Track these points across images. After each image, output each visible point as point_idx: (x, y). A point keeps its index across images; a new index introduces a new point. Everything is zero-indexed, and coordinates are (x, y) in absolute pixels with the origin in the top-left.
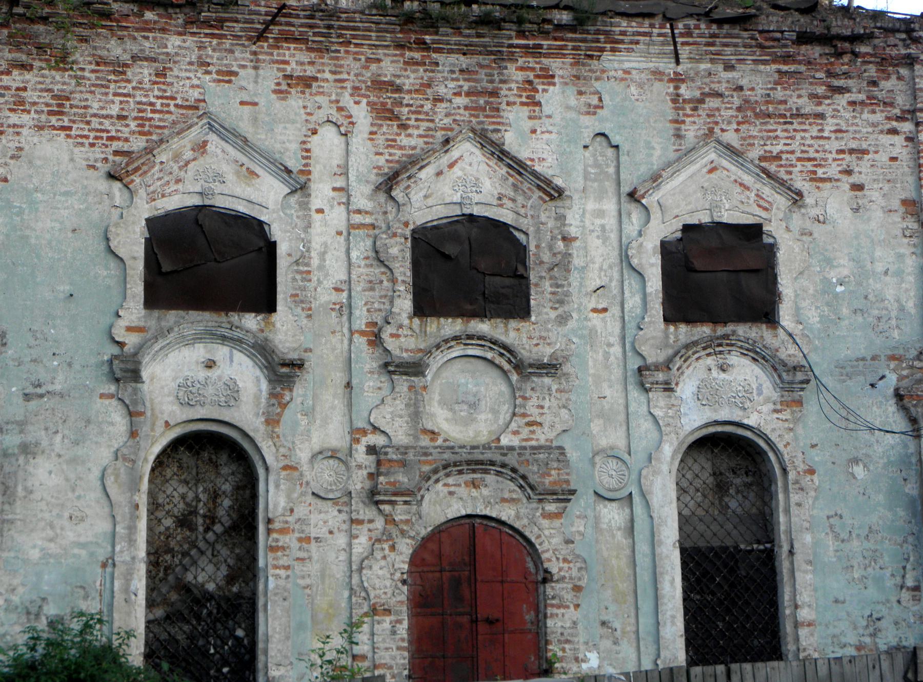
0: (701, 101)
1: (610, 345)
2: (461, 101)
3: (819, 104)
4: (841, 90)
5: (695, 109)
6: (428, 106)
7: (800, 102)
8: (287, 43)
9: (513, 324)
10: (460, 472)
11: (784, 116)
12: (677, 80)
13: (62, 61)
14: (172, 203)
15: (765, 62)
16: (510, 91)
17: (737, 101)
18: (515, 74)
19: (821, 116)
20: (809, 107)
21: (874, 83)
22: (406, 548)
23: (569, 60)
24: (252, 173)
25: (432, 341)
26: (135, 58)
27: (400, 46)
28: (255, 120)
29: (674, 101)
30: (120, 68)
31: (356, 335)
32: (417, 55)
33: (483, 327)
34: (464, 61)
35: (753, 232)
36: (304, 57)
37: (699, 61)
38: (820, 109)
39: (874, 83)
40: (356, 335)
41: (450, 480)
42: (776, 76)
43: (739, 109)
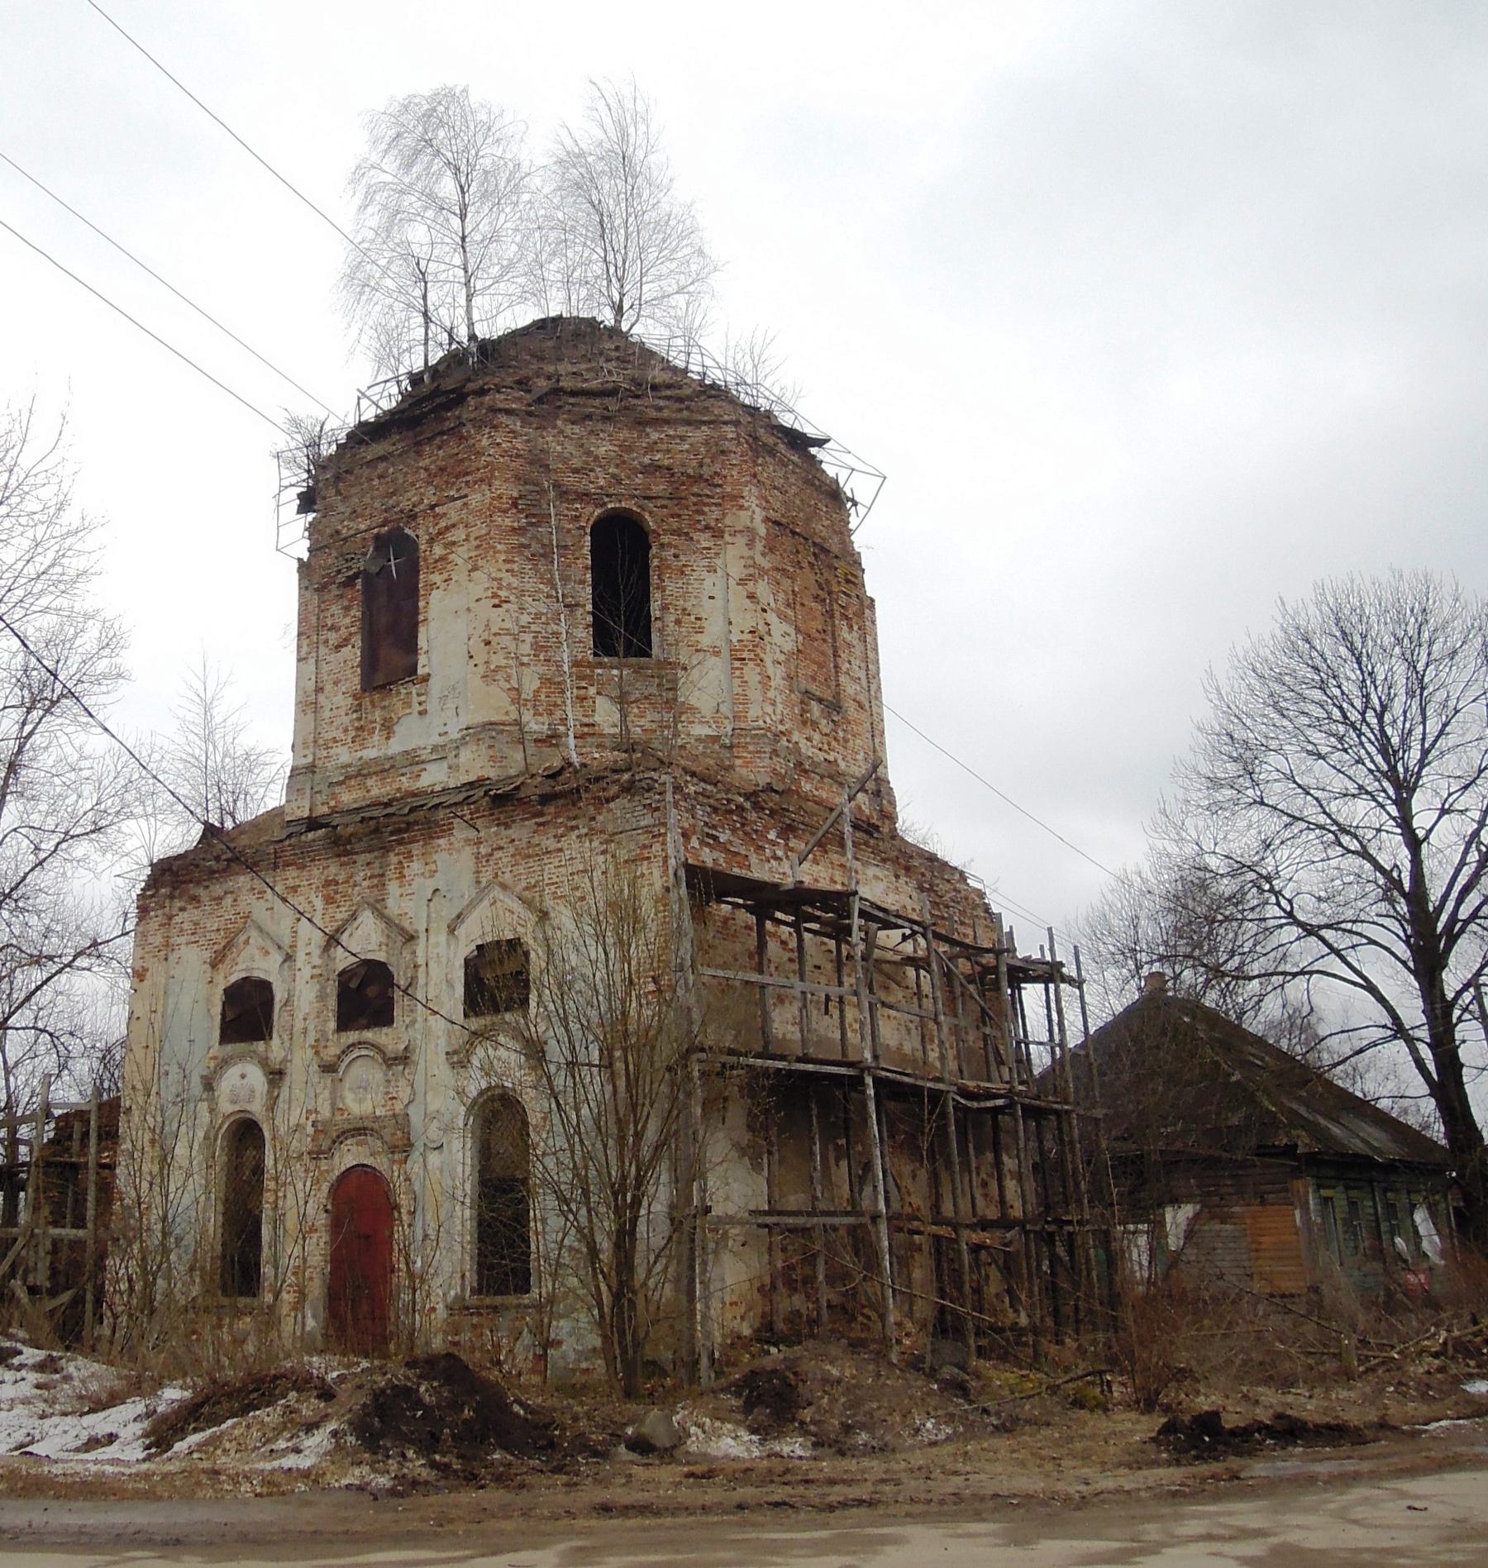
0: (491, 855)
1: (438, 1038)
2: (365, 883)
3: (559, 842)
4: (573, 828)
5: (487, 861)
6: (350, 890)
7: (548, 842)
8: (449, 410)
9: (385, 1030)
10: (353, 1136)
11: (537, 855)
12: (479, 843)
13: (195, 899)
14: (233, 979)
15: (527, 819)
16: (391, 873)
17: (512, 850)
18: (393, 859)
19: (561, 850)
20: (551, 844)
21: (593, 819)
22: (325, 1187)
23: (421, 843)
24: (267, 953)
25: (343, 1047)
26: (226, 893)
27: (339, 856)
28: (272, 918)
29: (477, 858)
30: (219, 900)
31: (403, 988)
32: (346, 859)
33: (368, 1035)
34: (368, 857)
35: (514, 944)
36: (295, 874)
37: (490, 827)
38: (559, 845)
39: (593, 819)
40: (403, 988)
41: (348, 1142)
42: (535, 827)
43: (513, 856)
